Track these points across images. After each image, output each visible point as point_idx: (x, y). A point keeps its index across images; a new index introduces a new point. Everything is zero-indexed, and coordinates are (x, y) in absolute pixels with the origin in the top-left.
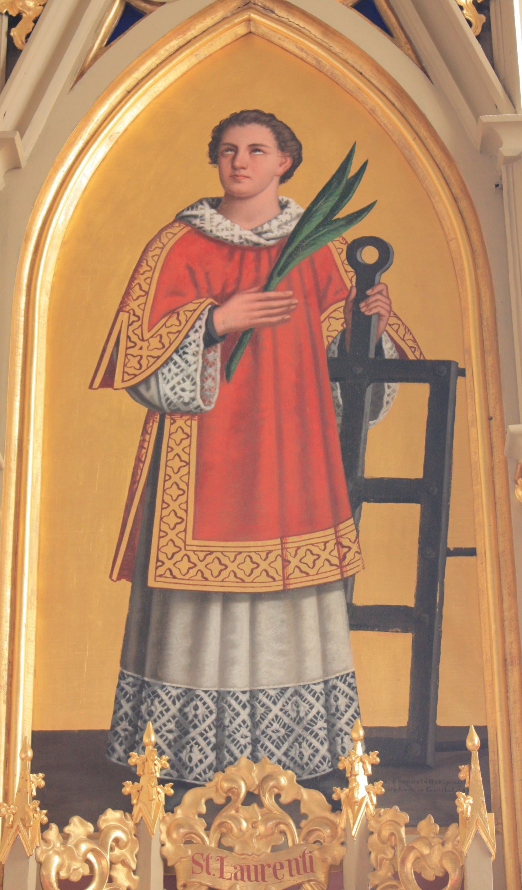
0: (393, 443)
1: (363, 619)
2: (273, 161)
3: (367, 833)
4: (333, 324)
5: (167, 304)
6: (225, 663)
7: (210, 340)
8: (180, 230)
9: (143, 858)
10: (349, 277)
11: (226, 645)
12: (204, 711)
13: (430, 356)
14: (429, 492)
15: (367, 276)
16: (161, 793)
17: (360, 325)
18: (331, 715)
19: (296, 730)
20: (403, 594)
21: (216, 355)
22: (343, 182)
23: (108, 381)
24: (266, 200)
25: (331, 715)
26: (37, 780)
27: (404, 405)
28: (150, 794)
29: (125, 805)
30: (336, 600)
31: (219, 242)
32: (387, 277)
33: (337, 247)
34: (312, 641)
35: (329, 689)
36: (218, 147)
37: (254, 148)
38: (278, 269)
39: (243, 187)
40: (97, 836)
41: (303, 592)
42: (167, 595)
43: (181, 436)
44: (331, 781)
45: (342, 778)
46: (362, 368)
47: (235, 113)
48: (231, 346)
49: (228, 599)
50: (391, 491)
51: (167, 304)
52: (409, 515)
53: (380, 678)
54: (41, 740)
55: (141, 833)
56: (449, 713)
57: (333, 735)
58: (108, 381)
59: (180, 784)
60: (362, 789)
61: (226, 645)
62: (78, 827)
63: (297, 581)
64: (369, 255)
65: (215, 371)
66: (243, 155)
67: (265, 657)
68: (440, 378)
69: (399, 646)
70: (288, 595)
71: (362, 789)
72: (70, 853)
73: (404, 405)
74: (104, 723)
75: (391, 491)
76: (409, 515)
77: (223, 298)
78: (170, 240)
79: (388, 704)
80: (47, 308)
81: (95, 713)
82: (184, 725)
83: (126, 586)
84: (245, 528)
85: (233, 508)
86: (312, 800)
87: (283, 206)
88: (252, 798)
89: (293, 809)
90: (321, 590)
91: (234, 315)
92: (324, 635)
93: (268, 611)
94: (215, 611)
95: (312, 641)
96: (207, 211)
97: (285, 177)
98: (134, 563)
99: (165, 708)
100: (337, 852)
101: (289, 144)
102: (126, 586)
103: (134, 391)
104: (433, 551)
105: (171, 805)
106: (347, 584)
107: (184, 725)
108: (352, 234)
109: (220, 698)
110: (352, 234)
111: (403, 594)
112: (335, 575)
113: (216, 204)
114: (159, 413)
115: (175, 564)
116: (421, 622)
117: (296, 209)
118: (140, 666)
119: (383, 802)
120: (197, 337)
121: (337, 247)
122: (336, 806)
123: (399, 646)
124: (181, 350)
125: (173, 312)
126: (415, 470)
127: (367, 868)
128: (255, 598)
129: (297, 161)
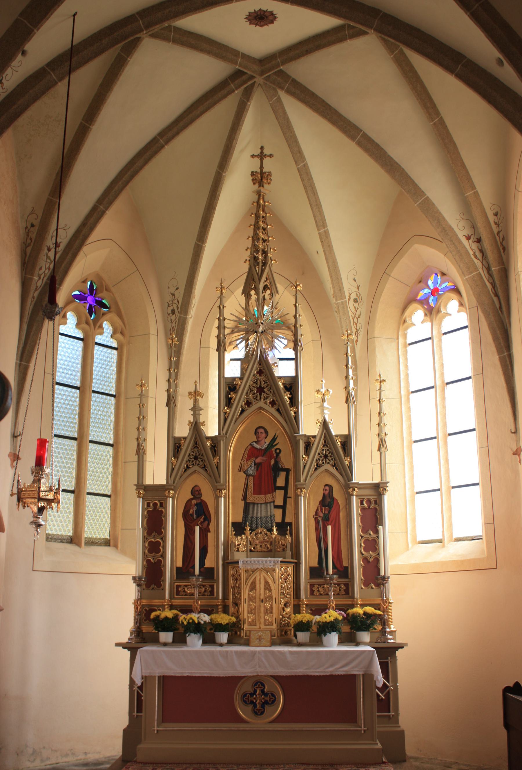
0: (280, 482)
1: (276, 507)
2: (264, 435)
3: (275, 538)
4: (272, 462)
5: (249, 459)
6: (257, 513)
7: (255, 464)
8: (250, 446)
9: (247, 541)
10: (275, 454)
11: (257, 510)
12: (254, 519)
13: (286, 467)
14: (285, 488)
15: (278, 454)
16: (249, 532)
17: (276, 463)
18: (271, 520)
19: (267, 522)
20: (281, 504)
21: (256, 467)
22: (274, 439)
23: (240, 471)
24: (263, 442)
25: (271, 520)
26: (234, 533)
27: (283, 474)
28: (248, 532)
29: (244, 534)
30: (272, 504)
31: (256, 448)
32: (280, 455)
33: (273, 450)
34: (269, 510)
35: (271, 517)
36: (256, 433)
37: (261, 433)
38: (265, 453)
39: (260, 439)
40: (242, 539)
41: (268, 503)
42: (249, 503)
43: (251, 479)
44: (270, 530)
45: (273, 531)
46: (277, 469)
47: (262, 26)
48: (258, 465)
49: (258, 504)
50: (280, 488)
51: (249, 459)
52: (282, 492)
53: (278, 515)
54: (233, 523)
55: (247, 537)
56: (287, 520)
57: (271, 523)
58: (240, 471)
59: (252, 530)
60: (275, 532)
61: (257, 510)
62: (239, 538)
63: (267, 501)
64: (278, 451)
65: (256, 469)
66: (260, 434)
67: (262, 512)
68: (287, 471)
69: (280, 511)
70: (266, 503)
71: (275, 532)
72: (238, 541)
73: (283, 474)
74: (241, 521)
75: (280, 488)
76: (282, 492)
77: (257, 458)
78: (249, 448)
79: (279, 519)
80: (248, 110)
81: (240, 519)
82: (252, 521)
83: (243, 502)
84: (260, 494)
85: (258, 491)
86: (269, 533)
87: (265, 443)
88: (261, 533)
89: (266, 534)
90: (270, 503)
91: (259, 460)
92: (271, 509)
93: (263, 506)
94: (256, 506)
95: (269, 510)
96: (254, 443)
97: (266, 438)
98: (245, 498)
99: (249, 519)
100: (271, 540)
101: (267, 433)
102: (243, 502)
103: (244, 472)
104: (286, 497)
105: (250, 533)
106: (274, 502)
107: (252, 521)
108: (275, 448)
109: (257, 518)
110: (275, 448)
111: (281, 504)
112: (272, 500)
113: (256, 442)
114: (248, 475)
115: (250, 499)
116: (283, 507)
117: (267, 443)
118: (246, 513)
119: (277, 534)
120: (253, 464)
121: (273, 450)
122: (272, 534)
123: (280, 511)
124: (251, 466)
125: (249, 460)
126: (283, 485)
127: (275, 542)
128: (261, 504)
129: (268, 435)
